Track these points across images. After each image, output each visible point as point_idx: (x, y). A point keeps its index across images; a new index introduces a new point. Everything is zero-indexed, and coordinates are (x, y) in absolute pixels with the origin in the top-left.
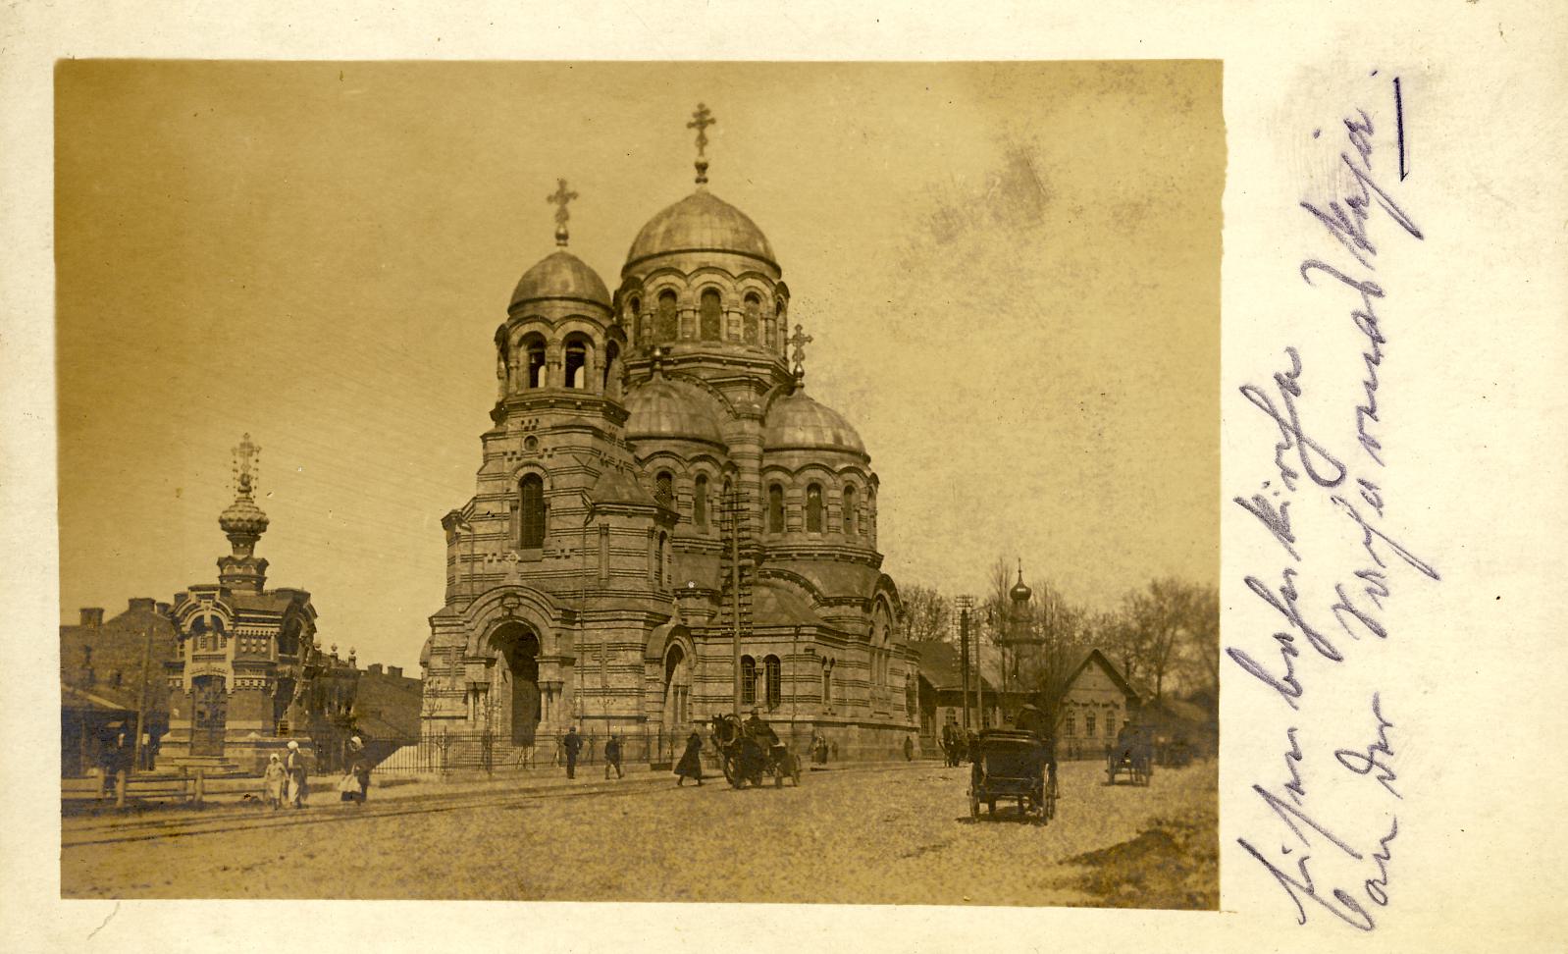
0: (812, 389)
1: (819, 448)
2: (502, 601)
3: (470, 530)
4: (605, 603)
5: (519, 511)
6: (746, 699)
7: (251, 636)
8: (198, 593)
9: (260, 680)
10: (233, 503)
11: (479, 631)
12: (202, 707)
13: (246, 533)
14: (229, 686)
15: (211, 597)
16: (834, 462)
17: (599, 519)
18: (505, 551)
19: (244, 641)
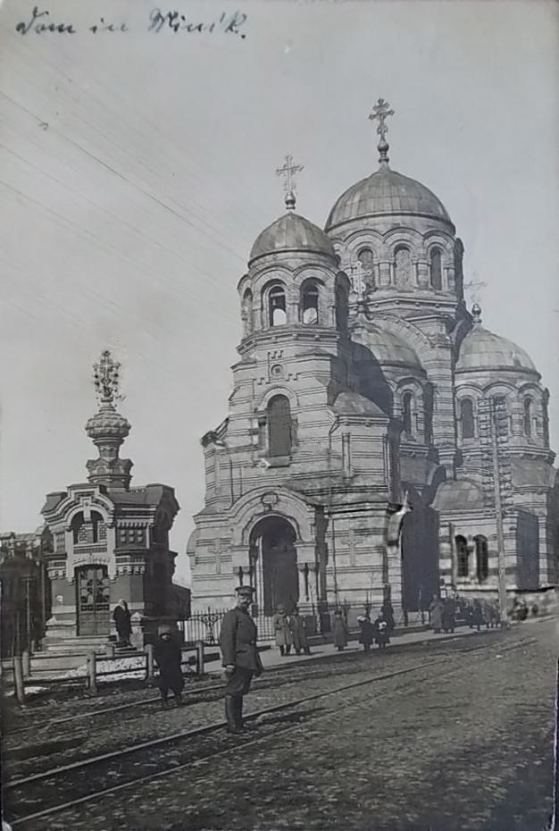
0: (487, 321)
1: (502, 369)
2: (262, 499)
3: (223, 445)
4: (350, 498)
5: (267, 426)
6: (461, 573)
7: (129, 528)
8: (77, 491)
9: (140, 566)
10: (98, 413)
11: (243, 524)
12: (84, 593)
13: (111, 436)
14: (111, 573)
15: (89, 494)
16: (515, 380)
17: (343, 429)
18: (255, 459)
19: (123, 532)
